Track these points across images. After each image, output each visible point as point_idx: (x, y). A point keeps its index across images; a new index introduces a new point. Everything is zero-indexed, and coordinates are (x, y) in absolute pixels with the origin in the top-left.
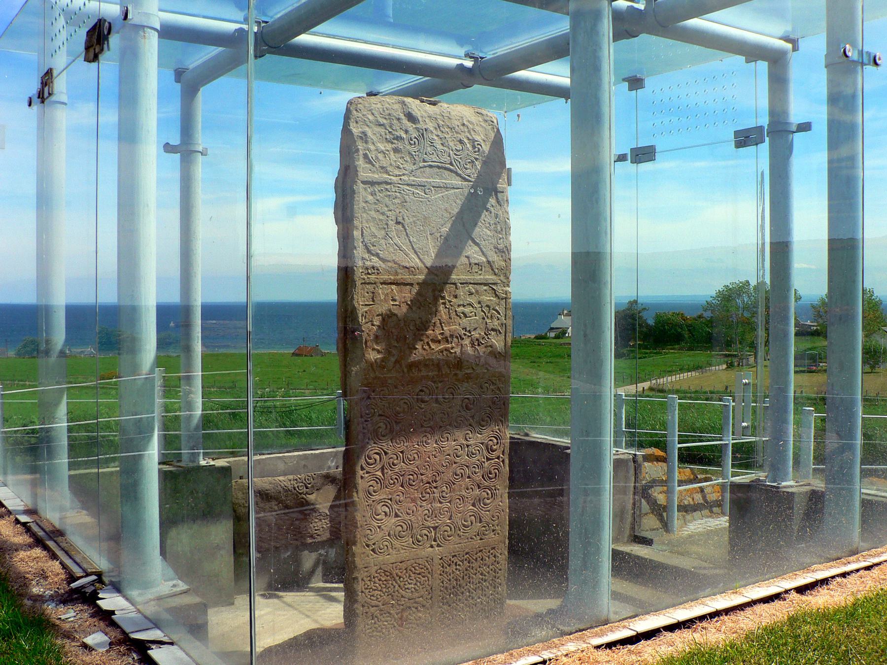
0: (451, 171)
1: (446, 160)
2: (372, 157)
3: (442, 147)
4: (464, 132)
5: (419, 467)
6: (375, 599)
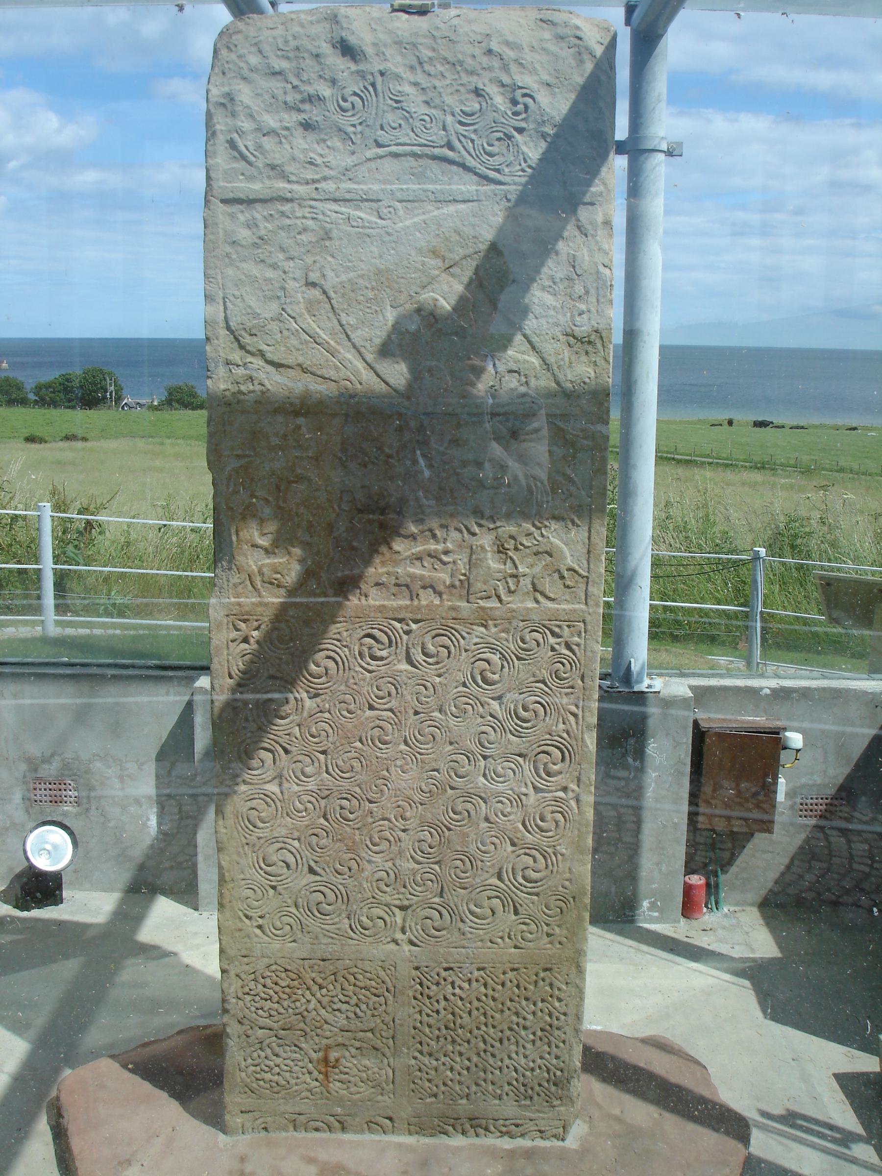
0: (451, 162)
1: (434, 138)
2: (246, 147)
3: (424, 109)
4: (490, 69)
5: (363, 786)
6: (266, 1015)
